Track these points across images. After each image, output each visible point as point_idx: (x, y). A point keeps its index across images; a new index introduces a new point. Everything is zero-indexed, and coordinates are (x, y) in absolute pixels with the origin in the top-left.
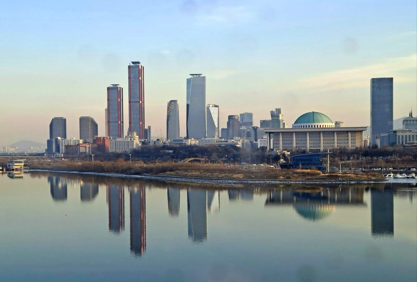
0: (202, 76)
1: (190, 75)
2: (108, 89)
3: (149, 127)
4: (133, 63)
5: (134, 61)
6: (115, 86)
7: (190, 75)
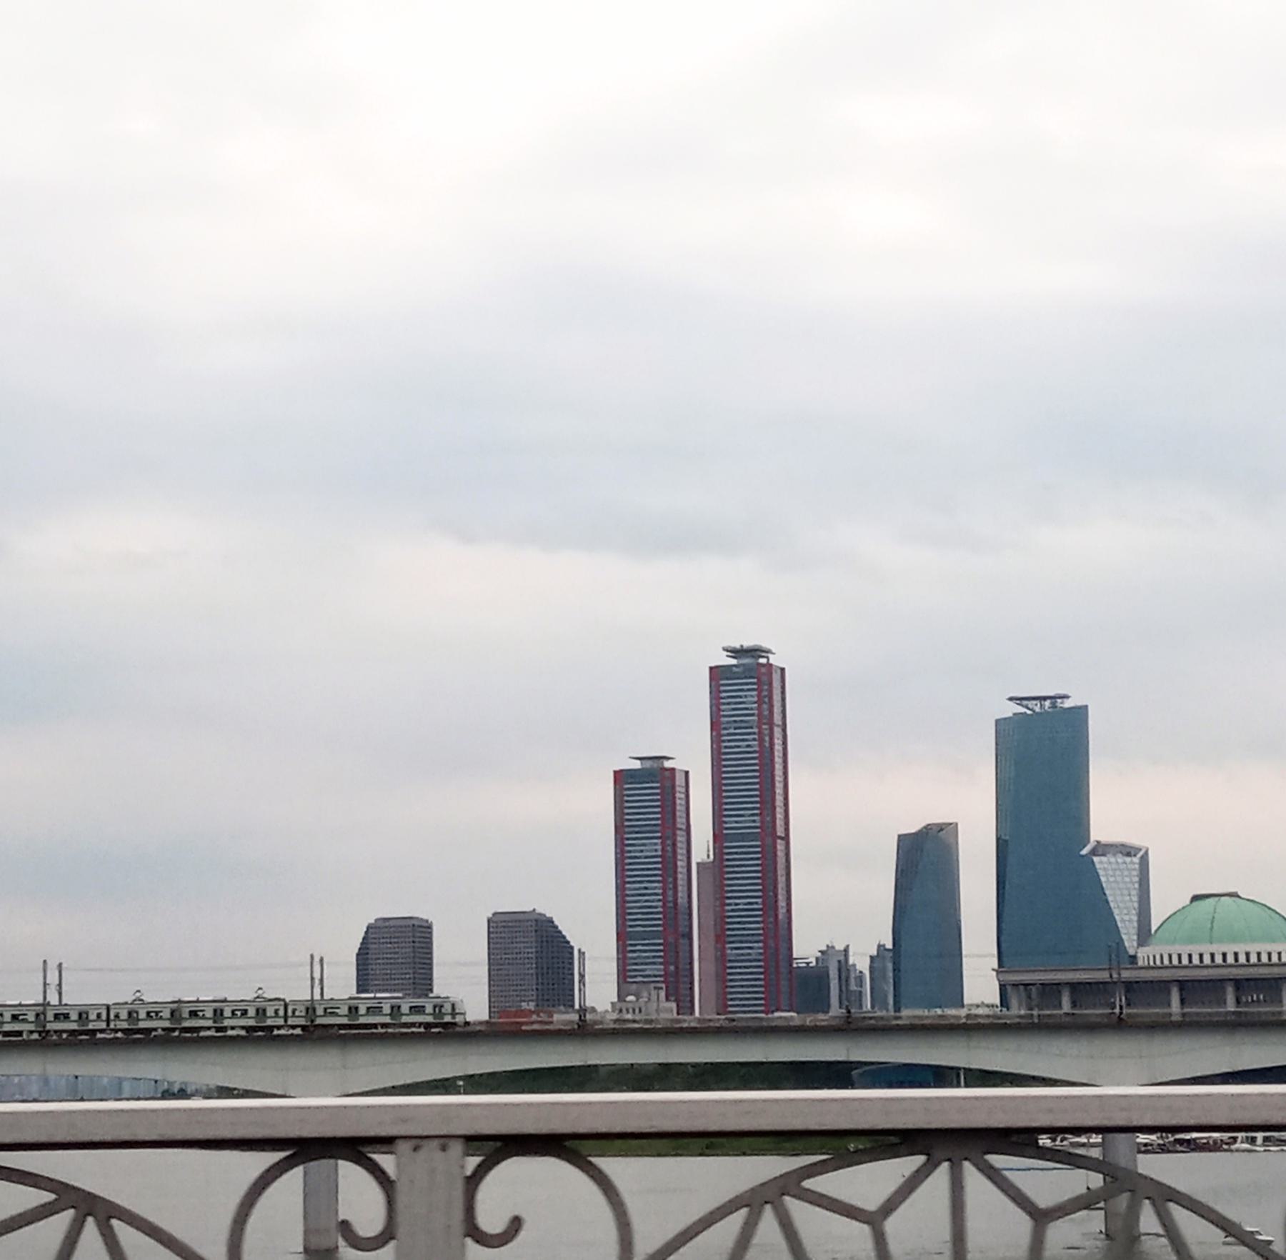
0: (1068, 704)
1: (1011, 699)
2: (621, 777)
3: (820, 951)
4: (736, 652)
5: (738, 646)
6: (648, 764)
7: (1011, 699)
